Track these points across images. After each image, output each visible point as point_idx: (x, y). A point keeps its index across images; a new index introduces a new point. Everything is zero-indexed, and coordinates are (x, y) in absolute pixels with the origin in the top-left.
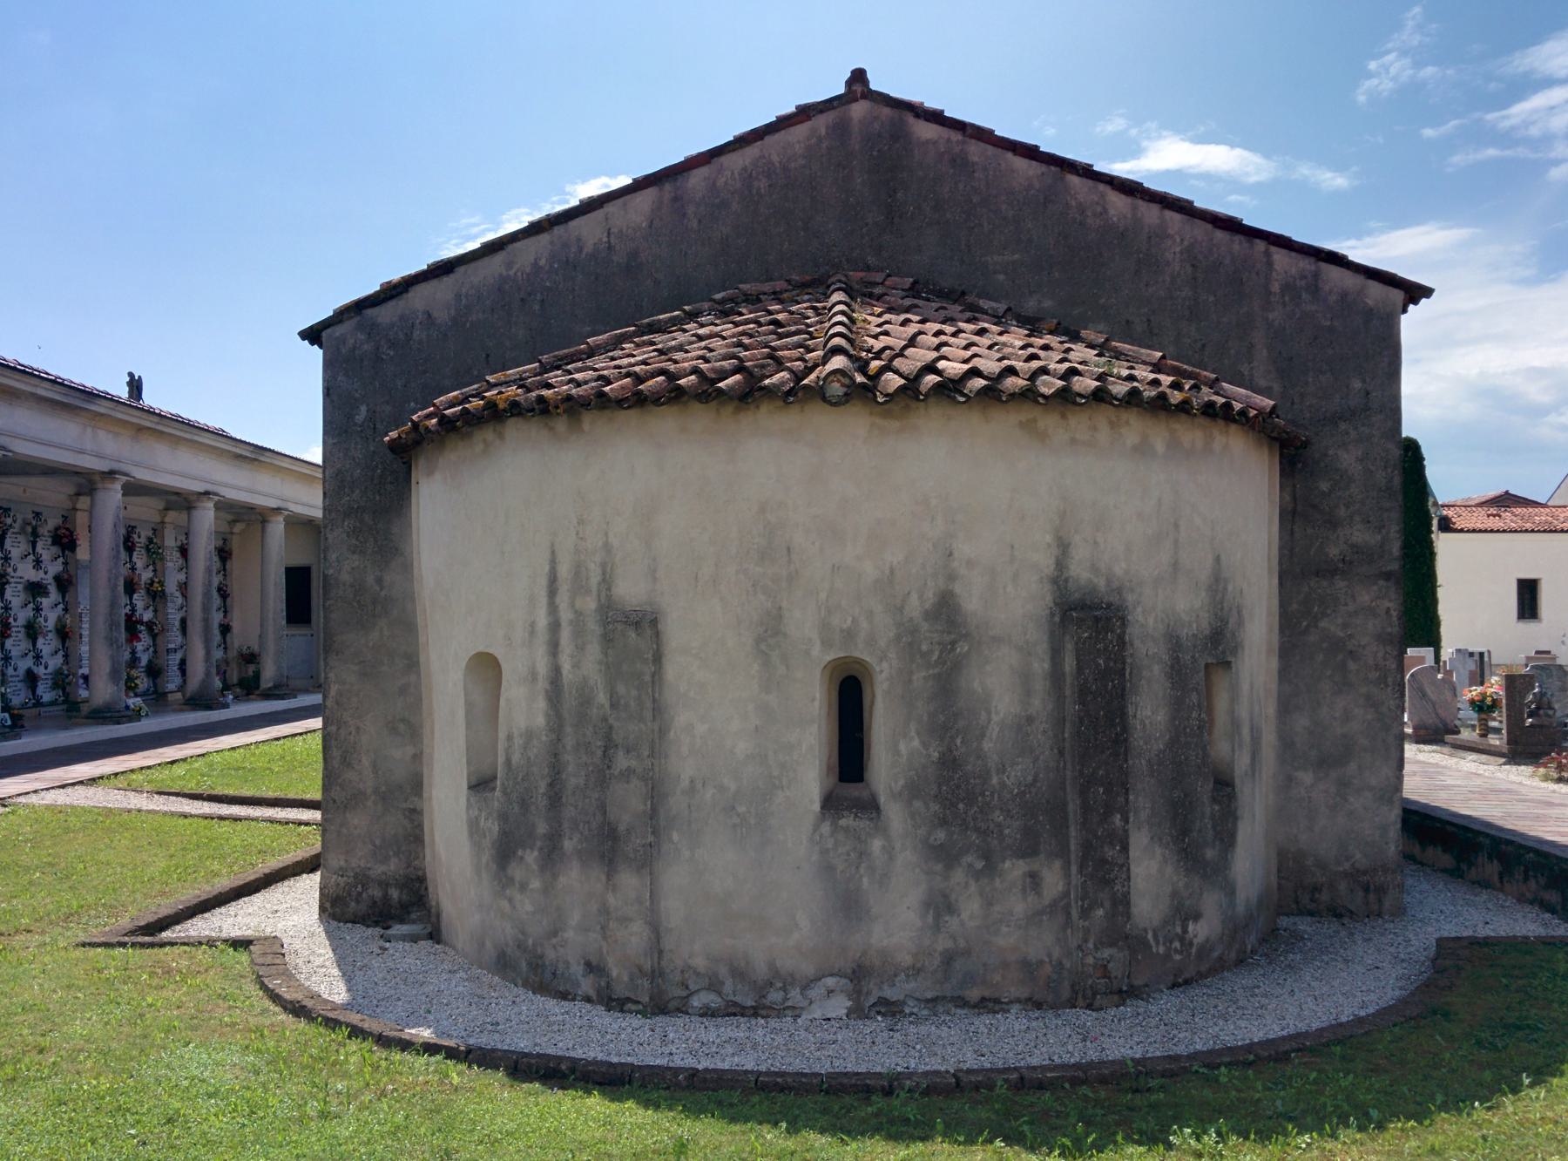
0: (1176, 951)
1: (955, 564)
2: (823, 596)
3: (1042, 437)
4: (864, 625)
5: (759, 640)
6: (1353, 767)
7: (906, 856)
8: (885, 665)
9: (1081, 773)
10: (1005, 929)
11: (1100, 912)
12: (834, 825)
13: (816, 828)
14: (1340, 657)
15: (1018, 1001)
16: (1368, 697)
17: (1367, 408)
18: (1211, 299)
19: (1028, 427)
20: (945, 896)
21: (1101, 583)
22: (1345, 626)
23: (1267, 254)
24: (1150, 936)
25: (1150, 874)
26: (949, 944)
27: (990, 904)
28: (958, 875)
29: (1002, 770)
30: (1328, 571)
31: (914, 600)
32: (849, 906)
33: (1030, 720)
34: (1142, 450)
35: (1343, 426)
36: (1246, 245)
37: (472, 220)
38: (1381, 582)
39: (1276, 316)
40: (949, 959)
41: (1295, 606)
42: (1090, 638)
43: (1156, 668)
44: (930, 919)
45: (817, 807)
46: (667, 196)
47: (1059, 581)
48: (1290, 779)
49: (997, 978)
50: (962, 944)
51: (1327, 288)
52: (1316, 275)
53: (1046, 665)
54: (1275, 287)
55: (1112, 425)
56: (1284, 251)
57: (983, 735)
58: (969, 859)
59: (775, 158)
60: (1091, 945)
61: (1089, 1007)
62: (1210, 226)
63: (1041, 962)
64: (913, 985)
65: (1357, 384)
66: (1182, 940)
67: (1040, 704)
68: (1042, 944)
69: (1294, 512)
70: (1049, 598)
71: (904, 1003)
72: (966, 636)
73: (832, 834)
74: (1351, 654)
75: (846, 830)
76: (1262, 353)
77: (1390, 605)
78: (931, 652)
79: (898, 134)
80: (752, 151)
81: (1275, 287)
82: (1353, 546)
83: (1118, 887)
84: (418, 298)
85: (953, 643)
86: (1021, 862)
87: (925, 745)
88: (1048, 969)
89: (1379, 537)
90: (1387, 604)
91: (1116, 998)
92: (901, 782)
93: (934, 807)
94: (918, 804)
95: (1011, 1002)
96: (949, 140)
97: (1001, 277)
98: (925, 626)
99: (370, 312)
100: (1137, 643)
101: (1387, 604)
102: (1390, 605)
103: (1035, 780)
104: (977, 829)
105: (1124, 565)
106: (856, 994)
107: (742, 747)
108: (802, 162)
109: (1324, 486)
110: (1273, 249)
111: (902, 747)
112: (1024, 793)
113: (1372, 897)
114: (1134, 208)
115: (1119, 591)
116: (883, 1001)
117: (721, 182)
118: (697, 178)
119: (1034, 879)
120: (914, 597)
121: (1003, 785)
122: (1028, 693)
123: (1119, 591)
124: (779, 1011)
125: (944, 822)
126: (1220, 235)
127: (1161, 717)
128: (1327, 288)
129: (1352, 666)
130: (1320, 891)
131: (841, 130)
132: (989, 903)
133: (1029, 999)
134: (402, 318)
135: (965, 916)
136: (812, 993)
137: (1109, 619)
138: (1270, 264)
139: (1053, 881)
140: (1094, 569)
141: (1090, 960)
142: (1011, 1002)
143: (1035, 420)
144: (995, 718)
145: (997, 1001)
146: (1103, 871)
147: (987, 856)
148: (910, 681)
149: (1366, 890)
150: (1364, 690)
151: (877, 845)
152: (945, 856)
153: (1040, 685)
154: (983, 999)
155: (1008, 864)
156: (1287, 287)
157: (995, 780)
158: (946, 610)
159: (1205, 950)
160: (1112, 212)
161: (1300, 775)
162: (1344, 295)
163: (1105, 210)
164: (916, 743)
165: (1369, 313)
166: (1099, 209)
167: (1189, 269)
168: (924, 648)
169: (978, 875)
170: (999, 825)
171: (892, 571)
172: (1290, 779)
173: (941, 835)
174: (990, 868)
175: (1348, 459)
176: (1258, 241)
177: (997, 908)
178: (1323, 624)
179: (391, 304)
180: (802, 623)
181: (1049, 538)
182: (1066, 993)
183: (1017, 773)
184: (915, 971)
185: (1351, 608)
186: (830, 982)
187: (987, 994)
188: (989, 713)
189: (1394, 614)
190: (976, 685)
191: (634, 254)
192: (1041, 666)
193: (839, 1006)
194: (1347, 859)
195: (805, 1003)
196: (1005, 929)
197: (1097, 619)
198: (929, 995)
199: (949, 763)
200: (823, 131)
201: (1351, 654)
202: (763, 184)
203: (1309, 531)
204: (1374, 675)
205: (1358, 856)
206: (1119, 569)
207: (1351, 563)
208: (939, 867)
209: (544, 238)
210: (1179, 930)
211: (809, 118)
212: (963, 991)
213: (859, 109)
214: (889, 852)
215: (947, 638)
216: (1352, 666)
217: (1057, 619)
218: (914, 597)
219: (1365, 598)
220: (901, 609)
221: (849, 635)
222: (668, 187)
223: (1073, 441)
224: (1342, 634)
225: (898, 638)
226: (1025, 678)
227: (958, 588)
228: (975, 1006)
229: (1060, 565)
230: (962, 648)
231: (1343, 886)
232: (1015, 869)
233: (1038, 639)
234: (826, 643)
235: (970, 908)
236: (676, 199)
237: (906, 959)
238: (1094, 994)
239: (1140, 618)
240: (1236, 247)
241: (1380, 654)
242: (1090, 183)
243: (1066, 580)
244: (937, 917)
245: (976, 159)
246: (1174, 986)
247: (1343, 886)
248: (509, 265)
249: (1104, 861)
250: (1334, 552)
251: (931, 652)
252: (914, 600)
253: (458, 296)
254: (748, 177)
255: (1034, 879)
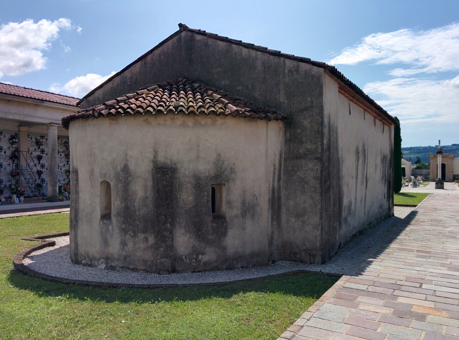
0: (193, 262)
1: (128, 157)
2: (100, 165)
3: (149, 123)
4: (108, 172)
5: (90, 176)
6: (306, 217)
7: (117, 231)
8: (112, 183)
9: (157, 212)
10: (138, 251)
11: (162, 249)
12: (103, 222)
13: (100, 222)
14: (303, 183)
15: (142, 270)
16: (311, 196)
17: (312, 106)
18: (269, 76)
19: (146, 121)
20: (125, 242)
21: (169, 162)
22: (304, 174)
23: (284, 61)
24: (184, 257)
25: (183, 241)
26: (126, 253)
27: (135, 244)
28: (128, 237)
29: (139, 210)
30: (299, 157)
31: (119, 167)
32: (105, 242)
33: (147, 198)
34: (184, 125)
35: (305, 112)
36: (278, 59)
37: (333, 53)
38: (315, 161)
39: (287, 80)
40: (126, 257)
41: (290, 168)
42: (161, 176)
43: (189, 185)
44: (122, 247)
45: (100, 217)
46: (143, 63)
47: (155, 161)
48: (288, 220)
49: (137, 263)
50: (128, 254)
51: (301, 70)
52: (298, 66)
53: (151, 184)
54: (286, 71)
55: (172, 119)
56: (289, 60)
57: (135, 201)
58: (130, 232)
59: (165, 50)
60: (159, 257)
61: (158, 273)
62: (269, 55)
63: (148, 261)
64: (118, 263)
65: (309, 99)
66: (196, 260)
67: (150, 193)
68: (148, 256)
69: (290, 140)
70: (152, 165)
71: (116, 267)
72: (131, 176)
73: (103, 224)
74: (306, 183)
75: (105, 223)
76: (282, 92)
77: (318, 168)
78: (122, 180)
79: (192, 39)
80: (160, 49)
81: (286, 71)
82: (307, 149)
83: (168, 243)
84: (97, 93)
85: (128, 177)
86: (143, 234)
87: (121, 203)
88: (150, 262)
89: (315, 146)
90: (317, 167)
91: (167, 272)
92: (116, 212)
93: (123, 219)
94: (119, 218)
95: (140, 270)
96: (204, 39)
97: (216, 76)
98: (121, 173)
99: (88, 98)
100: (181, 178)
101: (317, 167)
102: (318, 168)
103: (148, 213)
104: (132, 225)
105: (176, 157)
106: (107, 264)
107: (88, 202)
108: (171, 50)
109: (299, 131)
110: (286, 59)
111: (116, 204)
112: (144, 217)
113: (312, 258)
114: (249, 52)
115: (175, 164)
116: (111, 266)
117: (154, 58)
118: (149, 57)
119: (146, 239)
120: (119, 165)
121: (139, 214)
122: (146, 191)
123: (175, 164)
124: (95, 266)
125: (124, 223)
126: (272, 57)
127: (191, 198)
128: (301, 70)
129: (306, 186)
130: (297, 254)
131: (180, 40)
132: (135, 244)
133: (144, 270)
134: (94, 99)
135: (129, 247)
136: (99, 262)
137: (167, 171)
138: (285, 64)
139: (151, 240)
140: (166, 158)
141: (158, 261)
142: (140, 270)
143: (147, 119)
144: (138, 197)
145: (137, 269)
146: (164, 238)
147: (134, 232)
148: (118, 187)
149: (310, 255)
150: (309, 194)
151: (110, 227)
152: (124, 231)
153: (149, 188)
154: (133, 268)
155: (139, 235)
156: (290, 71)
157: (137, 213)
158: (126, 169)
159: (205, 264)
160: (243, 54)
161: (291, 219)
162: (306, 72)
163: (242, 54)
164: (119, 202)
165: (313, 76)
166: (240, 53)
167: (263, 68)
168: (121, 178)
169: (132, 237)
170: (137, 224)
171: (114, 159)
172: (288, 220)
173: (124, 226)
174: (135, 236)
175: (306, 123)
176: (282, 58)
177: (136, 246)
178: (298, 173)
179: (92, 96)
180: (97, 172)
181: (151, 150)
182: (154, 269)
183: (143, 211)
184: (118, 259)
185: (306, 168)
186: (102, 260)
187: (134, 267)
188: (136, 195)
189: (319, 170)
190: (133, 188)
191: (137, 79)
192: (150, 183)
193: (103, 266)
194: (305, 246)
195: (97, 265)
196: (138, 251)
197: (163, 172)
198: (121, 266)
199: (127, 208)
200: (175, 41)
201: (306, 183)
202: (162, 57)
203: (295, 145)
204: (312, 189)
205: (308, 245)
206: (175, 158)
207: (306, 154)
208: (123, 234)
209: (119, 77)
210: (195, 257)
211: (172, 38)
212: (128, 265)
213: (183, 34)
214: (113, 229)
215: (126, 176)
216: (306, 186)
217: (154, 171)
218: (119, 165)
219: (310, 165)
220: (116, 168)
221: (105, 175)
222: (143, 61)
223: (159, 124)
224: (303, 177)
225: (115, 175)
226: (145, 187)
227: (128, 163)
228: (132, 270)
229: (155, 157)
230: (130, 179)
231: (303, 254)
232: (141, 236)
233: (149, 176)
234: (101, 177)
235: (130, 245)
236: (145, 63)
237: (117, 257)
238: (160, 270)
239: (183, 171)
240: (276, 60)
241: (315, 183)
242: (238, 46)
243: (157, 161)
244: (123, 246)
245: (210, 43)
246: (194, 272)
247: (303, 254)
248: (113, 84)
249: (164, 236)
250: (301, 151)
251: (122, 180)
252: (119, 167)
253: (104, 93)
254: (160, 56)
255: (146, 239)
